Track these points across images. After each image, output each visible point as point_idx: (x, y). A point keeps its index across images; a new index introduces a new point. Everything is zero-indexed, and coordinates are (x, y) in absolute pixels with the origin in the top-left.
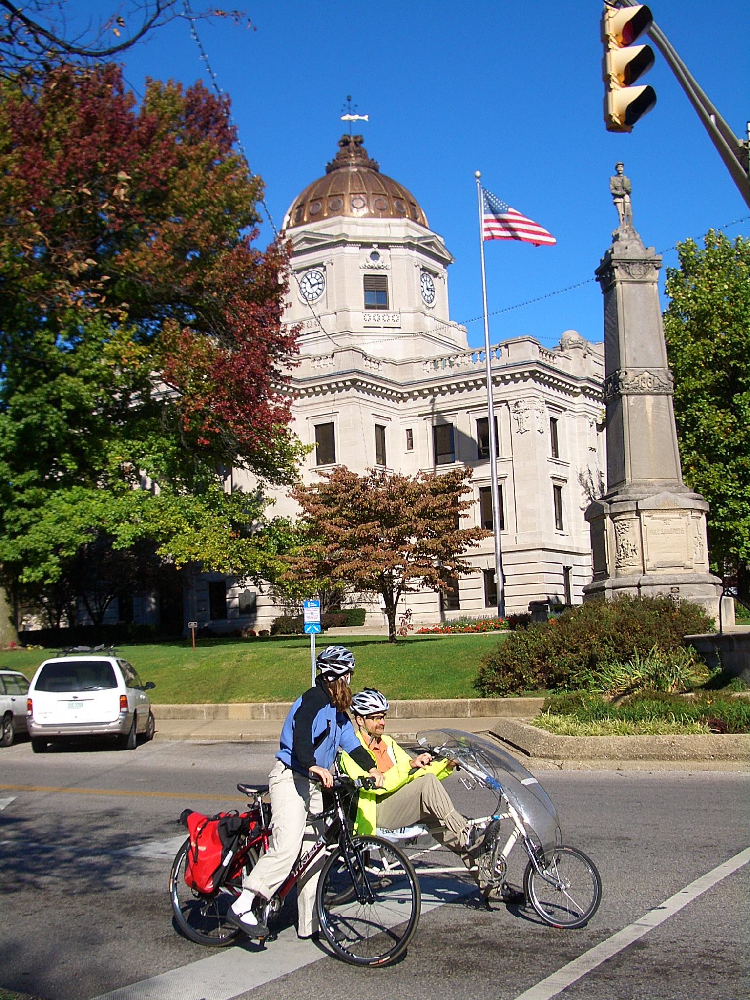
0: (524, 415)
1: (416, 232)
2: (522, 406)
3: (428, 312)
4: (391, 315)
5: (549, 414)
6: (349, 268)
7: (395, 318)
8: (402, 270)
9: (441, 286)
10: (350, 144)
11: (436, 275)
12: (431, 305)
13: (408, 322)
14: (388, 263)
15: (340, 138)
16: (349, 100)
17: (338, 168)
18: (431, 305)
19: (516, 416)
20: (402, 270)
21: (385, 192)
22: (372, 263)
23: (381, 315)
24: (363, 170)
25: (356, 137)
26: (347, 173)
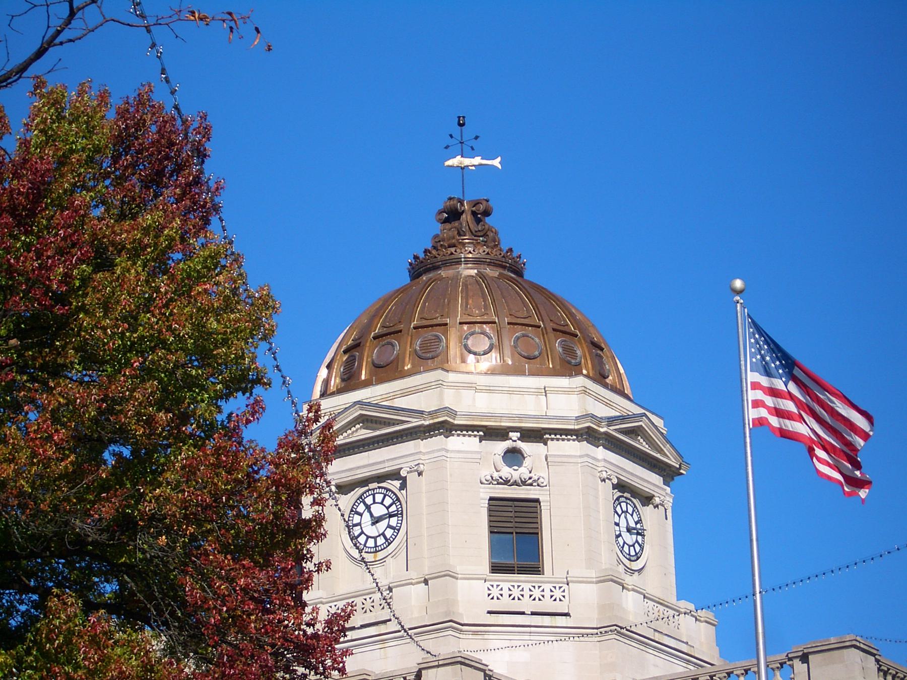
1: (604, 405)
3: (629, 580)
6: (456, 483)
7: (558, 594)
8: (572, 487)
9: (658, 524)
10: (464, 217)
11: (647, 500)
13: (585, 602)
14: (541, 472)
20: (572, 487)
22: (506, 472)
23: (527, 586)
24: (490, 272)
25: (476, 203)
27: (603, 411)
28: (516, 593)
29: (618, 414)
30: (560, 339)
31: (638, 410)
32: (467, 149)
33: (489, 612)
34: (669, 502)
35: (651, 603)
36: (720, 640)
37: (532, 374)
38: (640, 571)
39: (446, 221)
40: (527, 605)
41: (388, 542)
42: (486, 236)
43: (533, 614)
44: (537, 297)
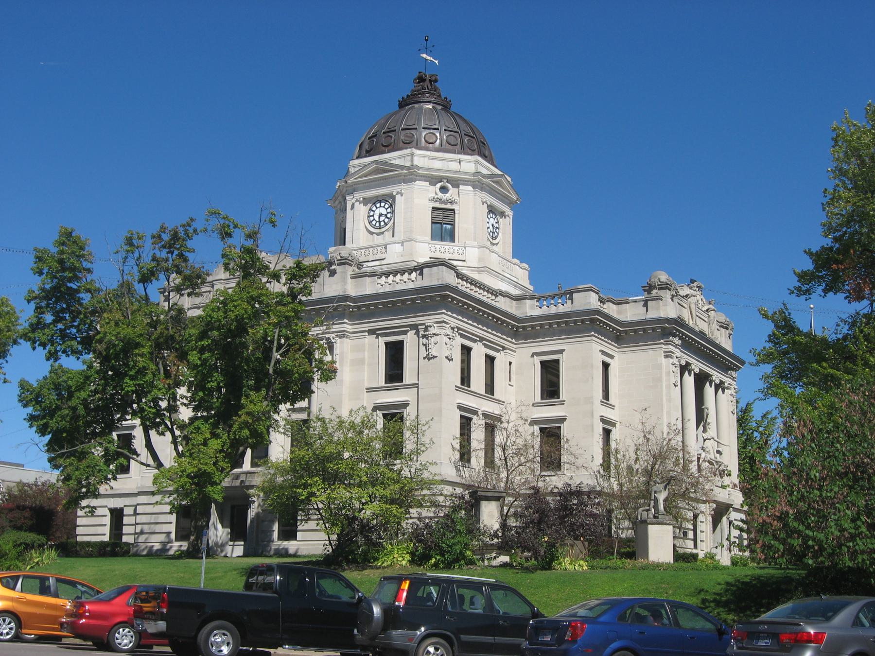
0: (433, 340)
2: (432, 331)
5: (459, 341)
6: (416, 202)
8: (470, 207)
9: (506, 225)
10: (425, 85)
11: (503, 214)
12: (494, 242)
14: (456, 197)
15: (417, 75)
16: (427, 40)
18: (494, 242)
19: (425, 341)
20: (470, 207)
21: (456, 129)
22: (440, 195)
23: (447, 247)
24: (439, 107)
26: (422, 108)
27: (485, 172)
30: (472, 142)
31: (500, 173)
32: (428, 52)
38: (497, 244)
39: (419, 82)
41: (386, 224)
42: (434, 92)
44: (458, 120)
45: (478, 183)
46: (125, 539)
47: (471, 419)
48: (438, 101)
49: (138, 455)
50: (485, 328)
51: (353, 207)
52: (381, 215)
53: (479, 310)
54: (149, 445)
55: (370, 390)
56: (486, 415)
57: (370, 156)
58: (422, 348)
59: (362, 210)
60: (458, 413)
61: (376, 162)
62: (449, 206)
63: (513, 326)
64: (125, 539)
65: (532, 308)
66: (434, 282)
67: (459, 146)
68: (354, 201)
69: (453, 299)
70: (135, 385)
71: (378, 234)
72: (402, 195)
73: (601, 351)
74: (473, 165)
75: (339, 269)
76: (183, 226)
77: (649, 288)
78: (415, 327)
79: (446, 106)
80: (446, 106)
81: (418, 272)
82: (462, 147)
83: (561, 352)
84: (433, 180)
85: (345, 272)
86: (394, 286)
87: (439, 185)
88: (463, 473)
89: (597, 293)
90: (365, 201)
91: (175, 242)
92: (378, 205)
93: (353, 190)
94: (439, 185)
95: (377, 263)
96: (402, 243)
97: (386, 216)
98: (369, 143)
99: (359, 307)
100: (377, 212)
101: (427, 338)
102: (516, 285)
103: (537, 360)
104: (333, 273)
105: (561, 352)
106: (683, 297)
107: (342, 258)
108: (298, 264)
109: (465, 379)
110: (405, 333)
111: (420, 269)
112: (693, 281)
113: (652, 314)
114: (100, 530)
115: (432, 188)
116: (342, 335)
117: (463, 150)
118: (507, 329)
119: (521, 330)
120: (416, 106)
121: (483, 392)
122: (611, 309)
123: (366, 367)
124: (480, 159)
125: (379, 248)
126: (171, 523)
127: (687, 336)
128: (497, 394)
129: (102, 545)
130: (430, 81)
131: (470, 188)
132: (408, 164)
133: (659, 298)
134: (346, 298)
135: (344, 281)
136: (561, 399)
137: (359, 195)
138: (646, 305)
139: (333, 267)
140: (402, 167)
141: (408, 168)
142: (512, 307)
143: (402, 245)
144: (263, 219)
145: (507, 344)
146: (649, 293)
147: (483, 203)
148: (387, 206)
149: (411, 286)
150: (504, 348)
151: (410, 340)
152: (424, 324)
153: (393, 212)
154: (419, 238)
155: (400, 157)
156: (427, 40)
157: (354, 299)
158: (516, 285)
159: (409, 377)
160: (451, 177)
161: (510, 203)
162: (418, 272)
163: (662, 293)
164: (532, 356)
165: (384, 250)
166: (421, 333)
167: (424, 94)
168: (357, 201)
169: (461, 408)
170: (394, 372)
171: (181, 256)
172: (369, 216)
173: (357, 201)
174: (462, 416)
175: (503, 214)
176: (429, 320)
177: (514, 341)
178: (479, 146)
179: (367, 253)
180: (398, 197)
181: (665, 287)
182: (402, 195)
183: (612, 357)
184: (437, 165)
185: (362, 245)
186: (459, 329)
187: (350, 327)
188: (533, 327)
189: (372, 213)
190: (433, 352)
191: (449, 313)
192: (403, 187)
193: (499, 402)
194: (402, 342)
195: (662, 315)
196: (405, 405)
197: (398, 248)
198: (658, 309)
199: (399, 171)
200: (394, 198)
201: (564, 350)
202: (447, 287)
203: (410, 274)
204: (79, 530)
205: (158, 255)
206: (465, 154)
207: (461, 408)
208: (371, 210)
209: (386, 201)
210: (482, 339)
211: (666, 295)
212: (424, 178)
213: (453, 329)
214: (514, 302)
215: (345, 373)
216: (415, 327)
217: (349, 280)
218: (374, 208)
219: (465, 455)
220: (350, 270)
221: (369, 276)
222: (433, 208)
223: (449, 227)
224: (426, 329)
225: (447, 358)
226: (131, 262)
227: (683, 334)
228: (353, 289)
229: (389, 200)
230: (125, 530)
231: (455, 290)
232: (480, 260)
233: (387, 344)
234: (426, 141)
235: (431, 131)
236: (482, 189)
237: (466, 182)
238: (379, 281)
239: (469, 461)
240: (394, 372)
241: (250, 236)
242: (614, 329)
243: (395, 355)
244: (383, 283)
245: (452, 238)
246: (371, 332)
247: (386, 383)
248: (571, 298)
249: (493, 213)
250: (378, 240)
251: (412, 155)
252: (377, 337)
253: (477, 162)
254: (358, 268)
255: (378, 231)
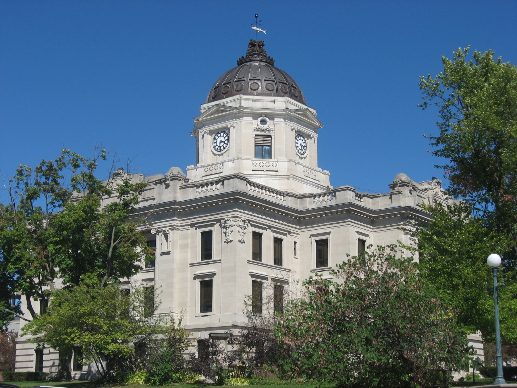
1: (294, 105)
2: (229, 223)
3: (301, 161)
4: (271, 163)
5: (251, 229)
6: (244, 131)
7: (275, 165)
8: (282, 133)
10: (256, 48)
12: (302, 156)
13: (283, 167)
14: (272, 127)
15: (249, 42)
16: (256, 17)
17: (251, 61)
18: (302, 156)
19: (224, 230)
20: (282, 133)
21: (273, 79)
22: (261, 126)
23: (265, 162)
24: (264, 64)
25: (259, 42)
27: (293, 107)
28: (268, 165)
29: (298, 108)
33: (253, 170)
34: (316, 136)
35: (306, 168)
36: (331, 180)
37: (226, 97)
38: (305, 158)
40: (265, 168)
41: (224, 148)
42: (262, 53)
43: (267, 171)
45: (288, 116)
46: (45, 370)
47: (261, 284)
48: (264, 59)
49: (23, 314)
50: (273, 219)
51: (203, 137)
52: (221, 142)
53: (266, 207)
54: (30, 307)
55: (192, 265)
56: (274, 280)
57: (214, 101)
58: (224, 235)
59: (209, 138)
60: (250, 280)
61: (217, 105)
62: (267, 133)
63: (296, 217)
64: (45, 370)
65: (310, 203)
66: (231, 190)
67: (275, 91)
68: (203, 133)
69: (243, 201)
70: (16, 268)
71: (219, 155)
72: (234, 127)
73: (357, 232)
74: (284, 103)
75: (171, 183)
76: (56, 161)
77: (393, 186)
78: (218, 221)
79: (270, 62)
80: (270, 62)
81: (221, 183)
82: (277, 91)
83: (328, 233)
84: (255, 116)
85: (175, 185)
86: (206, 193)
87: (260, 119)
88: (254, 320)
89: (354, 191)
90: (211, 133)
91: (50, 171)
92: (219, 135)
93: (203, 125)
94: (260, 119)
95: (217, 176)
96: (233, 161)
97: (224, 142)
98: (215, 92)
99: (184, 209)
100: (219, 140)
101: (226, 228)
102: (322, 187)
103: (313, 240)
104: (167, 186)
105: (328, 233)
106: (422, 190)
107: (174, 176)
108: (126, 183)
109: (257, 255)
110: (213, 225)
111: (222, 181)
112: (433, 178)
113: (395, 204)
114: (29, 364)
115: (255, 121)
116: (173, 228)
117: (278, 94)
118: (291, 219)
119: (303, 219)
120: (248, 64)
121: (272, 263)
122: (367, 203)
123: (189, 250)
124: (289, 99)
125: (219, 165)
126: (32, 361)
127: (422, 218)
128: (285, 265)
129: (30, 374)
130: (259, 46)
131: (282, 120)
132: (238, 105)
133: (400, 193)
134: (174, 203)
135: (175, 192)
136: (329, 267)
137: (207, 129)
138: (391, 198)
139: (167, 182)
140: (233, 108)
141: (237, 108)
142: (296, 204)
143: (233, 163)
144: (97, 154)
145: (292, 230)
146: (394, 189)
147: (292, 130)
148: (225, 136)
149: (217, 192)
150: (289, 233)
151: (216, 229)
152: (223, 219)
153: (228, 140)
154: (245, 157)
155: (233, 101)
156: (256, 17)
157: (180, 204)
158: (318, 186)
159: (215, 256)
160: (268, 113)
161: (315, 129)
162: (221, 183)
163: (402, 189)
164: (310, 237)
165: (222, 166)
166: (223, 225)
167: (253, 55)
168: (205, 133)
169: (252, 275)
170: (207, 253)
171: (55, 181)
172: (214, 143)
173: (205, 133)
174: (253, 281)
175: (309, 136)
176: (227, 216)
177: (298, 227)
178: (290, 90)
179: (211, 169)
180: (231, 129)
181: (404, 184)
182: (234, 127)
183: (367, 236)
184: (259, 105)
185: (209, 163)
186: (250, 221)
187: (179, 222)
188: (310, 217)
189: (215, 141)
190: (230, 238)
191: (242, 211)
192: (234, 122)
193: (195, 278)
194: (211, 232)
195: (402, 204)
196: (213, 275)
197: (230, 164)
198: (399, 200)
199: (232, 111)
200: (229, 129)
201: (330, 232)
202: (237, 193)
203: (216, 185)
204: (17, 365)
205: (39, 180)
206: (278, 96)
207: (252, 275)
208: (215, 139)
209: (224, 132)
210: (270, 227)
211: (406, 190)
212: (248, 115)
213: (244, 221)
214: (299, 200)
215: (177, 255)
216: (218, 221)
217: (179, 190)
218: (217, 138)
219: (257, 308)
220: (179, 184)
221: (191, 187)
222: (256, 135)
223: (268, 147)
224: (225, 223)
225: (240, 241)
226: (22, 186)
227: (419, 217)
228: (181, 196)
229: (225, 131)
230: (45, 364)
231: (244, 195)
232: (289, 170)
233: (202, 233)
234: (251, 89)
235: (256, 81)
236: (291, 120)
237: (279, 116)
238: (198, 190)
239: (261, 311)
240: (207, 253)
241: (90, 166)
242: (367, 216)
243: (207, 239)
244: (200, 191)
245: (270, 156)
246: (192, 225)
247: (202, 260)
248: (335, 196)
249: (301, 136)
250: (220, 159)
251: (240, 99)
252: (196, 229)
253: (286, 101)
254: (185, 182)
255: (219, 153)
